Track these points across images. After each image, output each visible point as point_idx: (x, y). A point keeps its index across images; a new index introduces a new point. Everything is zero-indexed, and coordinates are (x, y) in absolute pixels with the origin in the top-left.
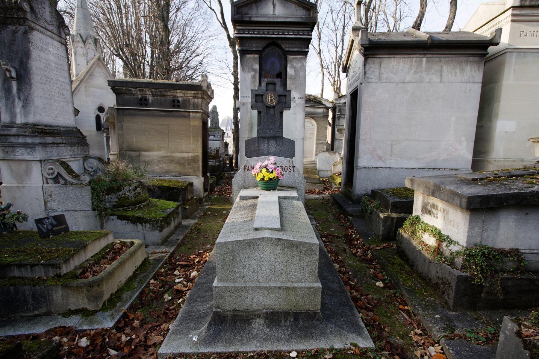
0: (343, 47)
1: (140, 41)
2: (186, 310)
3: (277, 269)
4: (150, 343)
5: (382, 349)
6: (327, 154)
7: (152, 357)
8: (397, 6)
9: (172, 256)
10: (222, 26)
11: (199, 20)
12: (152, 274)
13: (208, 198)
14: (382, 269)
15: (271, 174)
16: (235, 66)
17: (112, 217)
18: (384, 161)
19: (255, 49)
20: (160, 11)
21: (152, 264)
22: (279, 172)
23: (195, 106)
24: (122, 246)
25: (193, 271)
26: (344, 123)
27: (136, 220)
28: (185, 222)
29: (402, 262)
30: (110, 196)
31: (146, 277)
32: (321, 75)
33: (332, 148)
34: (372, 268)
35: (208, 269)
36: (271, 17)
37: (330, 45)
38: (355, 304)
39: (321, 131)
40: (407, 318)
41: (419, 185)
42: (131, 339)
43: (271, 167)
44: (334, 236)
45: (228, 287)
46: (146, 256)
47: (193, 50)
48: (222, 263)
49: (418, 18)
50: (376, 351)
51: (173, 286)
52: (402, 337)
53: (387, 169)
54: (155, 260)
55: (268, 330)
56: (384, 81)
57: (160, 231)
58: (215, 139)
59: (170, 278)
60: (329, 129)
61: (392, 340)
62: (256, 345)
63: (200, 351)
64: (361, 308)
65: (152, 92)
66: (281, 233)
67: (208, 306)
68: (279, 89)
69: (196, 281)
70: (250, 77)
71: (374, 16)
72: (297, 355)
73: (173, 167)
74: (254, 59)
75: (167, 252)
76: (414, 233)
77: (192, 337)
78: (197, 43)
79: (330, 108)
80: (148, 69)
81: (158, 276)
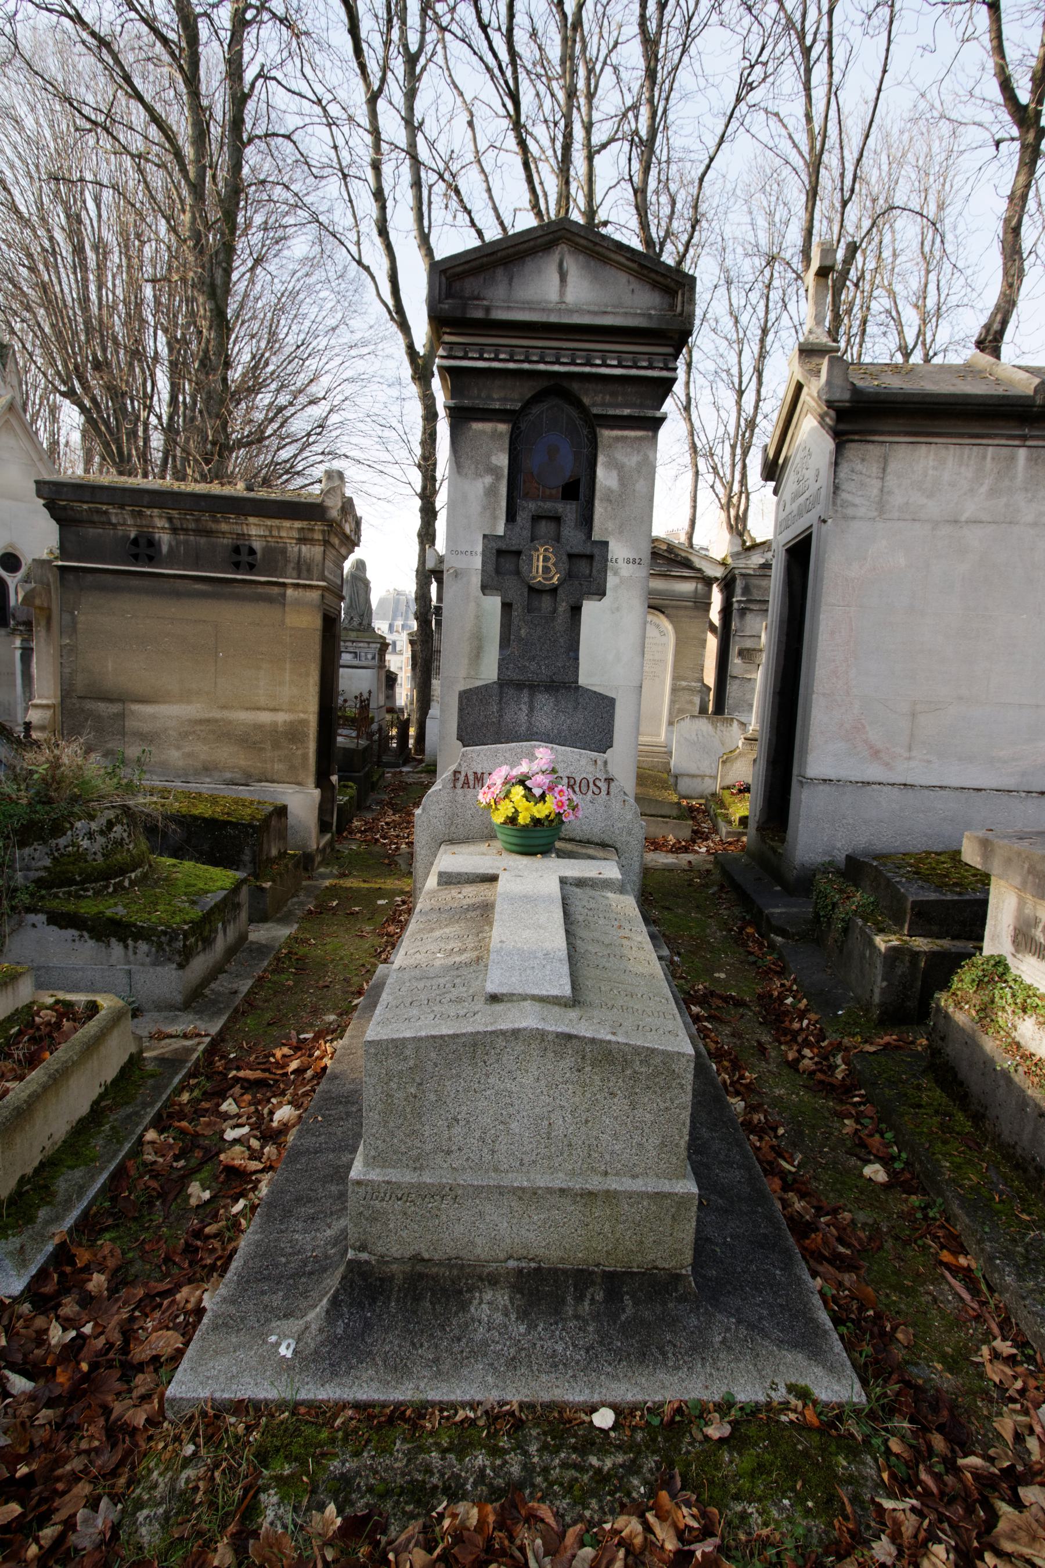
0: (758, 392)
1: (137, 354)
2: (258, 1244)
3: (559, 1131)
4: (140, 1353)
5: (891, 1410)
6: (703, 725)
7: (146, 1407)
8: (928, 272)
9: (214, 1048)
10: (392, 319)
11: (322, 295)
12: (152, 1112)
13: (331, 854)
14: (881, 1120)
15: (540, 805)
16: (429, 439)
17: (32, 918)
18: (887, 764)
19: (497, 406)
20: (203, 267)
21: (152, 1076)
22: (564, 798)
23: (303, 568)
24: (61, 1016)
25: (280, 1105)
26: (762, 632)
27: (107, 930)
28: (260, 934)
29: (945, 1100)
30: (27, 851)
31: (132, 1119)
32: (690, 475)
33: (720, 704)
34: (849, 1116)
35: (329, 1100)
36: (551, 311)
37: (721, 384)
38: (798, 1241)
39: (687, 650)
40: (966, 1296)
41: (1008, 861)
42: (80, 1336)
43: (539, 783)
44: (726, 999)
45: (399, 1185)
46: (133, 1049)
47: (299, 384)
48: (380, 1106)
49: (994, 315)
50: (872, 1415)
51: (218, 1154)
52: (952, 1365)
53: (896, 789)
54: (161, 1060)
55: (522, 1329)
56: (896, 515)
57: (181, 966)
58: (356, 662)
59: (208, 1124)
60: (712, 642)
61: (919, 1374)
62: (484, 1382)
63: (303, 1395)
64: (820, 1258)
65: (170, 519)
66: (573, 1014)
67: (329, 1232)
68: (571, 535)
69: (290, 1138)
70: (481, 491)
71: (858, 301)
72: (616, 1422)
73: (227, 755)
74: (495, 435)
75: (199, 1035)
76: (986, 1012)
77: (278, 1344)
78: (312, 364)
79: (716, 579)
80: (157, 441)
81: (170, 1116)
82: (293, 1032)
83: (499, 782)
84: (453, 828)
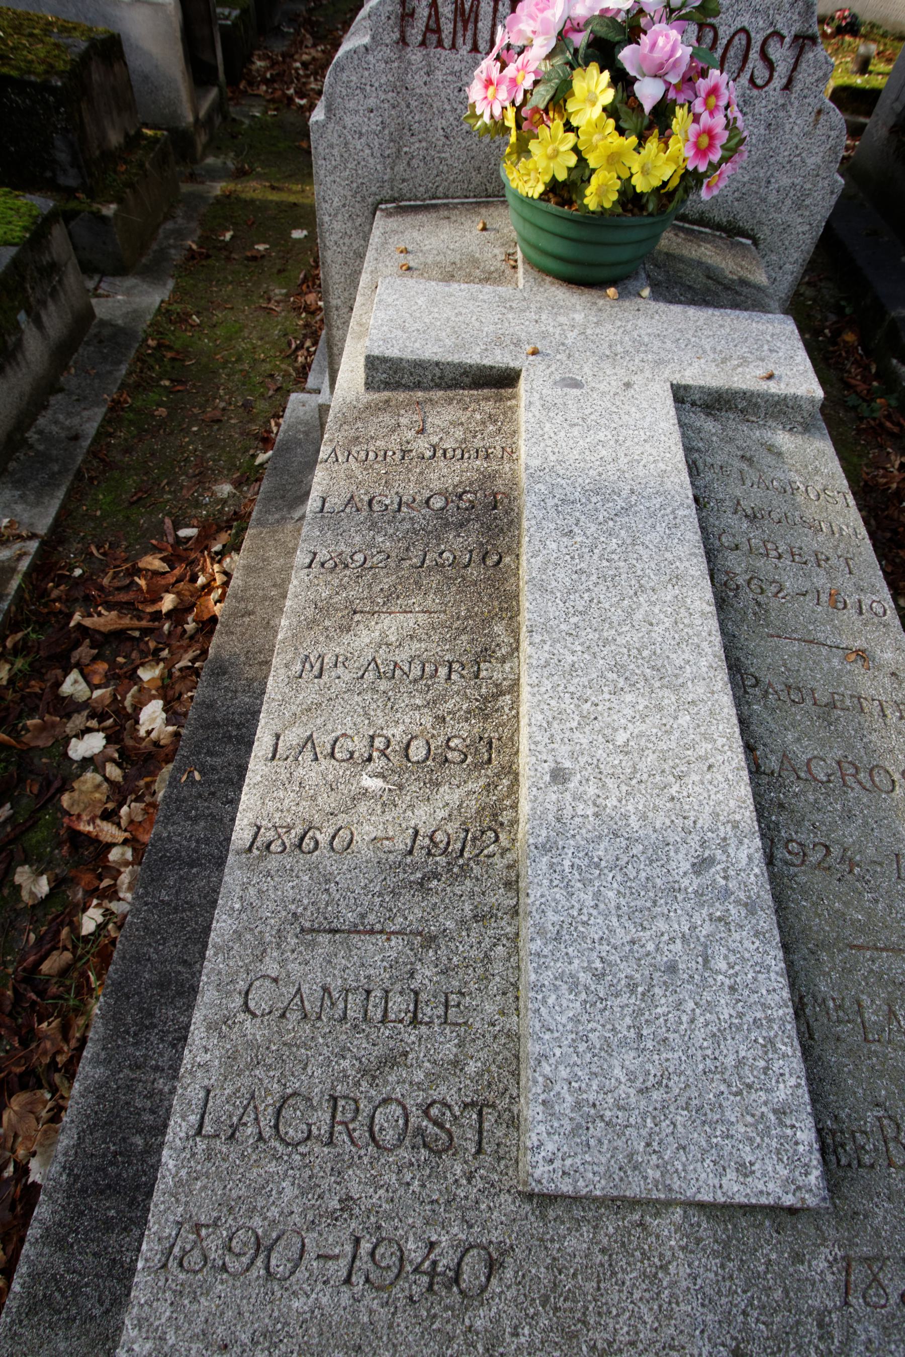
13: (221, 129)
82: (168, 522)
83: (541, 47)
84: (401, 167)
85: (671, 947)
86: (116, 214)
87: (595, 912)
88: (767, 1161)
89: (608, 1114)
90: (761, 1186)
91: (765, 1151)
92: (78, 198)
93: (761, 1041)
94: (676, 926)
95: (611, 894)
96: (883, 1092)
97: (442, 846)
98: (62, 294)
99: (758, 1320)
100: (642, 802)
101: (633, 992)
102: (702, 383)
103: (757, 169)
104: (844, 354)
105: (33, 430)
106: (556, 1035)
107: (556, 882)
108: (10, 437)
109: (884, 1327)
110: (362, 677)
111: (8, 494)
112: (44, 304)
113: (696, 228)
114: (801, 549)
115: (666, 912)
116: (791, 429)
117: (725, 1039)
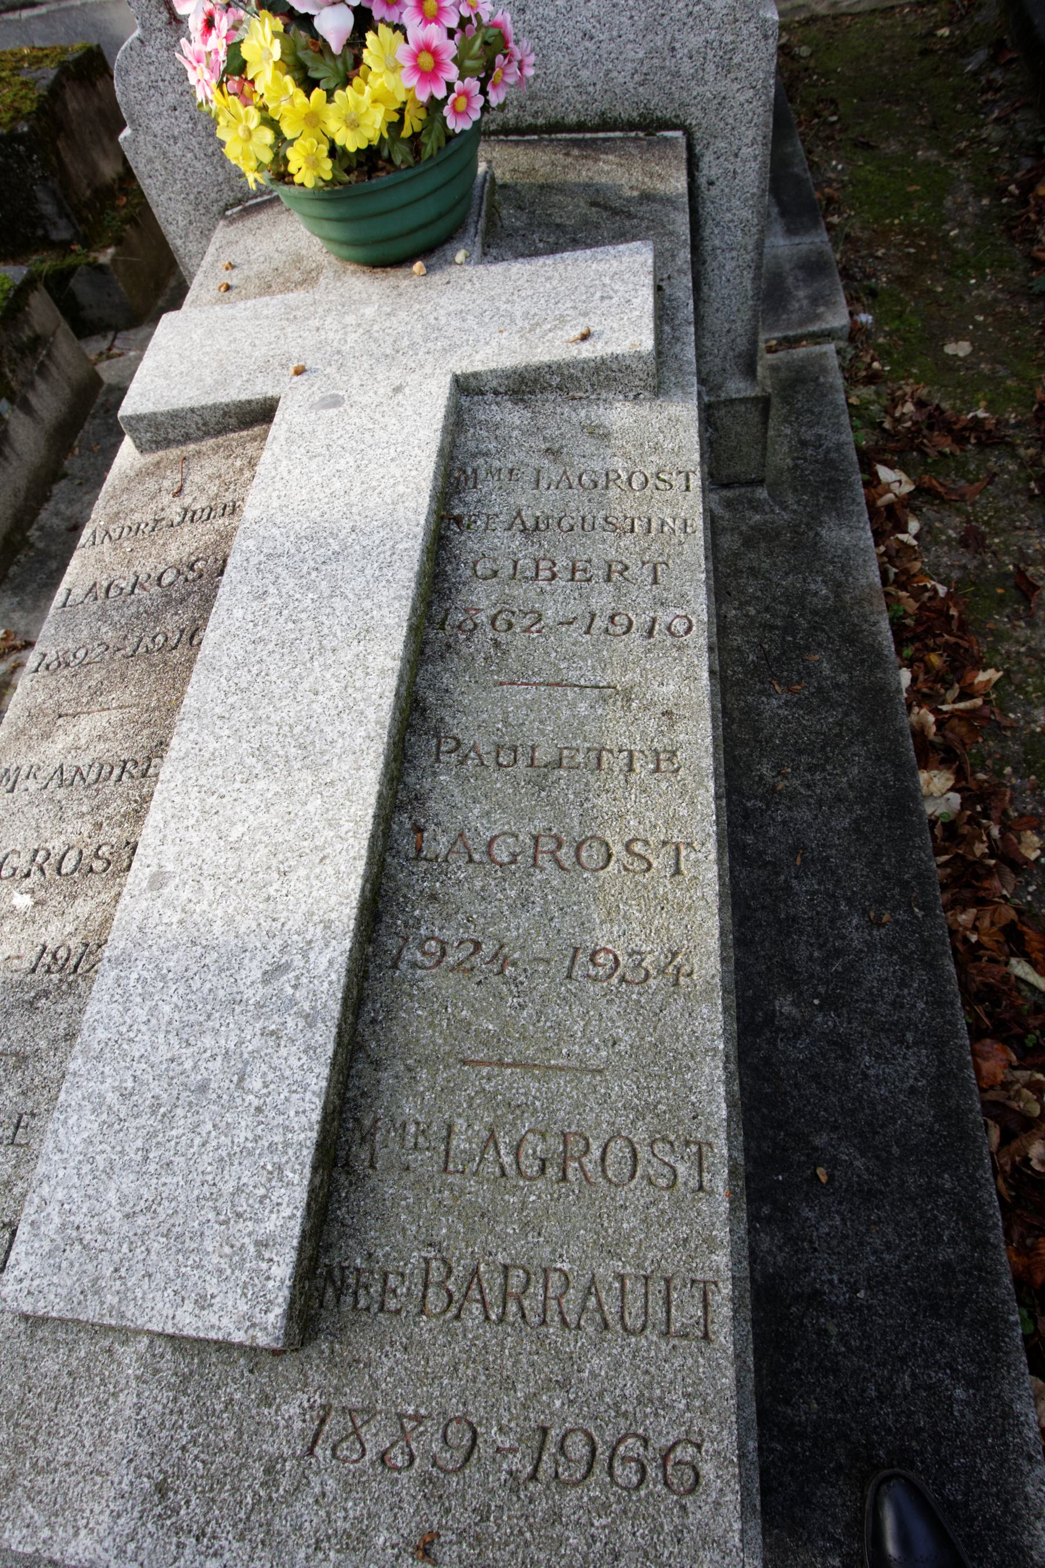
85: (210, 1065)
86: (114, 260)
87: (144, 1028)
88: (229, 1295)
89: (88, 1237)
90: (214, 1320)
91: (232, 1284)
92: (72, 251)
93: (269, 1167)
94: (222, 1042)
95: (167, 1009)
96: (444, 1231)
97: (60, 962)
98: (53, 369)
99: (196, 1457)
100: (234, 904)
101: (154, 1113)
102: (493, 365)
103: (649, 37)
104: (1033, 217)
105: (35, 526)
106: (66, 1155)
107: (117, 997)
108: (7, 539)
109: (346, 1483)
110: (46, 787)
111: (8, 602)
112: (31, 385)
113: (601, 135)
114: (589, 561)
115: (217, 1026)
116: (636, 397)
117: (232, 1164)
